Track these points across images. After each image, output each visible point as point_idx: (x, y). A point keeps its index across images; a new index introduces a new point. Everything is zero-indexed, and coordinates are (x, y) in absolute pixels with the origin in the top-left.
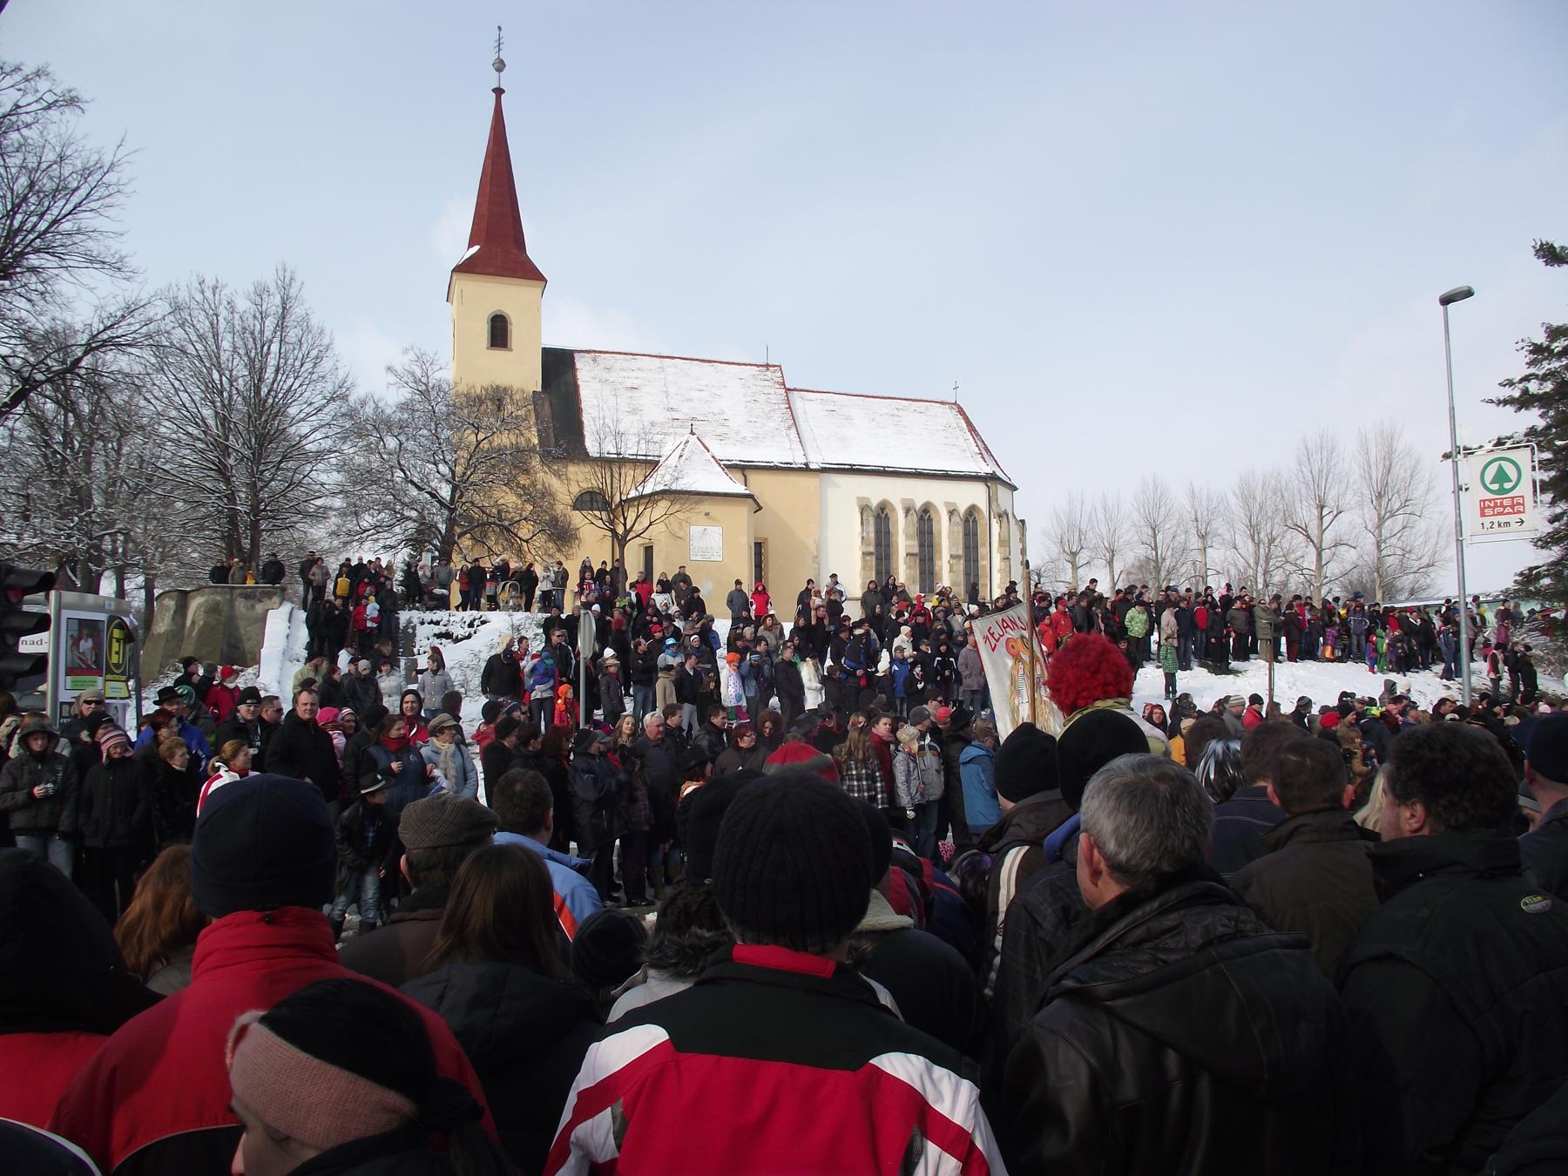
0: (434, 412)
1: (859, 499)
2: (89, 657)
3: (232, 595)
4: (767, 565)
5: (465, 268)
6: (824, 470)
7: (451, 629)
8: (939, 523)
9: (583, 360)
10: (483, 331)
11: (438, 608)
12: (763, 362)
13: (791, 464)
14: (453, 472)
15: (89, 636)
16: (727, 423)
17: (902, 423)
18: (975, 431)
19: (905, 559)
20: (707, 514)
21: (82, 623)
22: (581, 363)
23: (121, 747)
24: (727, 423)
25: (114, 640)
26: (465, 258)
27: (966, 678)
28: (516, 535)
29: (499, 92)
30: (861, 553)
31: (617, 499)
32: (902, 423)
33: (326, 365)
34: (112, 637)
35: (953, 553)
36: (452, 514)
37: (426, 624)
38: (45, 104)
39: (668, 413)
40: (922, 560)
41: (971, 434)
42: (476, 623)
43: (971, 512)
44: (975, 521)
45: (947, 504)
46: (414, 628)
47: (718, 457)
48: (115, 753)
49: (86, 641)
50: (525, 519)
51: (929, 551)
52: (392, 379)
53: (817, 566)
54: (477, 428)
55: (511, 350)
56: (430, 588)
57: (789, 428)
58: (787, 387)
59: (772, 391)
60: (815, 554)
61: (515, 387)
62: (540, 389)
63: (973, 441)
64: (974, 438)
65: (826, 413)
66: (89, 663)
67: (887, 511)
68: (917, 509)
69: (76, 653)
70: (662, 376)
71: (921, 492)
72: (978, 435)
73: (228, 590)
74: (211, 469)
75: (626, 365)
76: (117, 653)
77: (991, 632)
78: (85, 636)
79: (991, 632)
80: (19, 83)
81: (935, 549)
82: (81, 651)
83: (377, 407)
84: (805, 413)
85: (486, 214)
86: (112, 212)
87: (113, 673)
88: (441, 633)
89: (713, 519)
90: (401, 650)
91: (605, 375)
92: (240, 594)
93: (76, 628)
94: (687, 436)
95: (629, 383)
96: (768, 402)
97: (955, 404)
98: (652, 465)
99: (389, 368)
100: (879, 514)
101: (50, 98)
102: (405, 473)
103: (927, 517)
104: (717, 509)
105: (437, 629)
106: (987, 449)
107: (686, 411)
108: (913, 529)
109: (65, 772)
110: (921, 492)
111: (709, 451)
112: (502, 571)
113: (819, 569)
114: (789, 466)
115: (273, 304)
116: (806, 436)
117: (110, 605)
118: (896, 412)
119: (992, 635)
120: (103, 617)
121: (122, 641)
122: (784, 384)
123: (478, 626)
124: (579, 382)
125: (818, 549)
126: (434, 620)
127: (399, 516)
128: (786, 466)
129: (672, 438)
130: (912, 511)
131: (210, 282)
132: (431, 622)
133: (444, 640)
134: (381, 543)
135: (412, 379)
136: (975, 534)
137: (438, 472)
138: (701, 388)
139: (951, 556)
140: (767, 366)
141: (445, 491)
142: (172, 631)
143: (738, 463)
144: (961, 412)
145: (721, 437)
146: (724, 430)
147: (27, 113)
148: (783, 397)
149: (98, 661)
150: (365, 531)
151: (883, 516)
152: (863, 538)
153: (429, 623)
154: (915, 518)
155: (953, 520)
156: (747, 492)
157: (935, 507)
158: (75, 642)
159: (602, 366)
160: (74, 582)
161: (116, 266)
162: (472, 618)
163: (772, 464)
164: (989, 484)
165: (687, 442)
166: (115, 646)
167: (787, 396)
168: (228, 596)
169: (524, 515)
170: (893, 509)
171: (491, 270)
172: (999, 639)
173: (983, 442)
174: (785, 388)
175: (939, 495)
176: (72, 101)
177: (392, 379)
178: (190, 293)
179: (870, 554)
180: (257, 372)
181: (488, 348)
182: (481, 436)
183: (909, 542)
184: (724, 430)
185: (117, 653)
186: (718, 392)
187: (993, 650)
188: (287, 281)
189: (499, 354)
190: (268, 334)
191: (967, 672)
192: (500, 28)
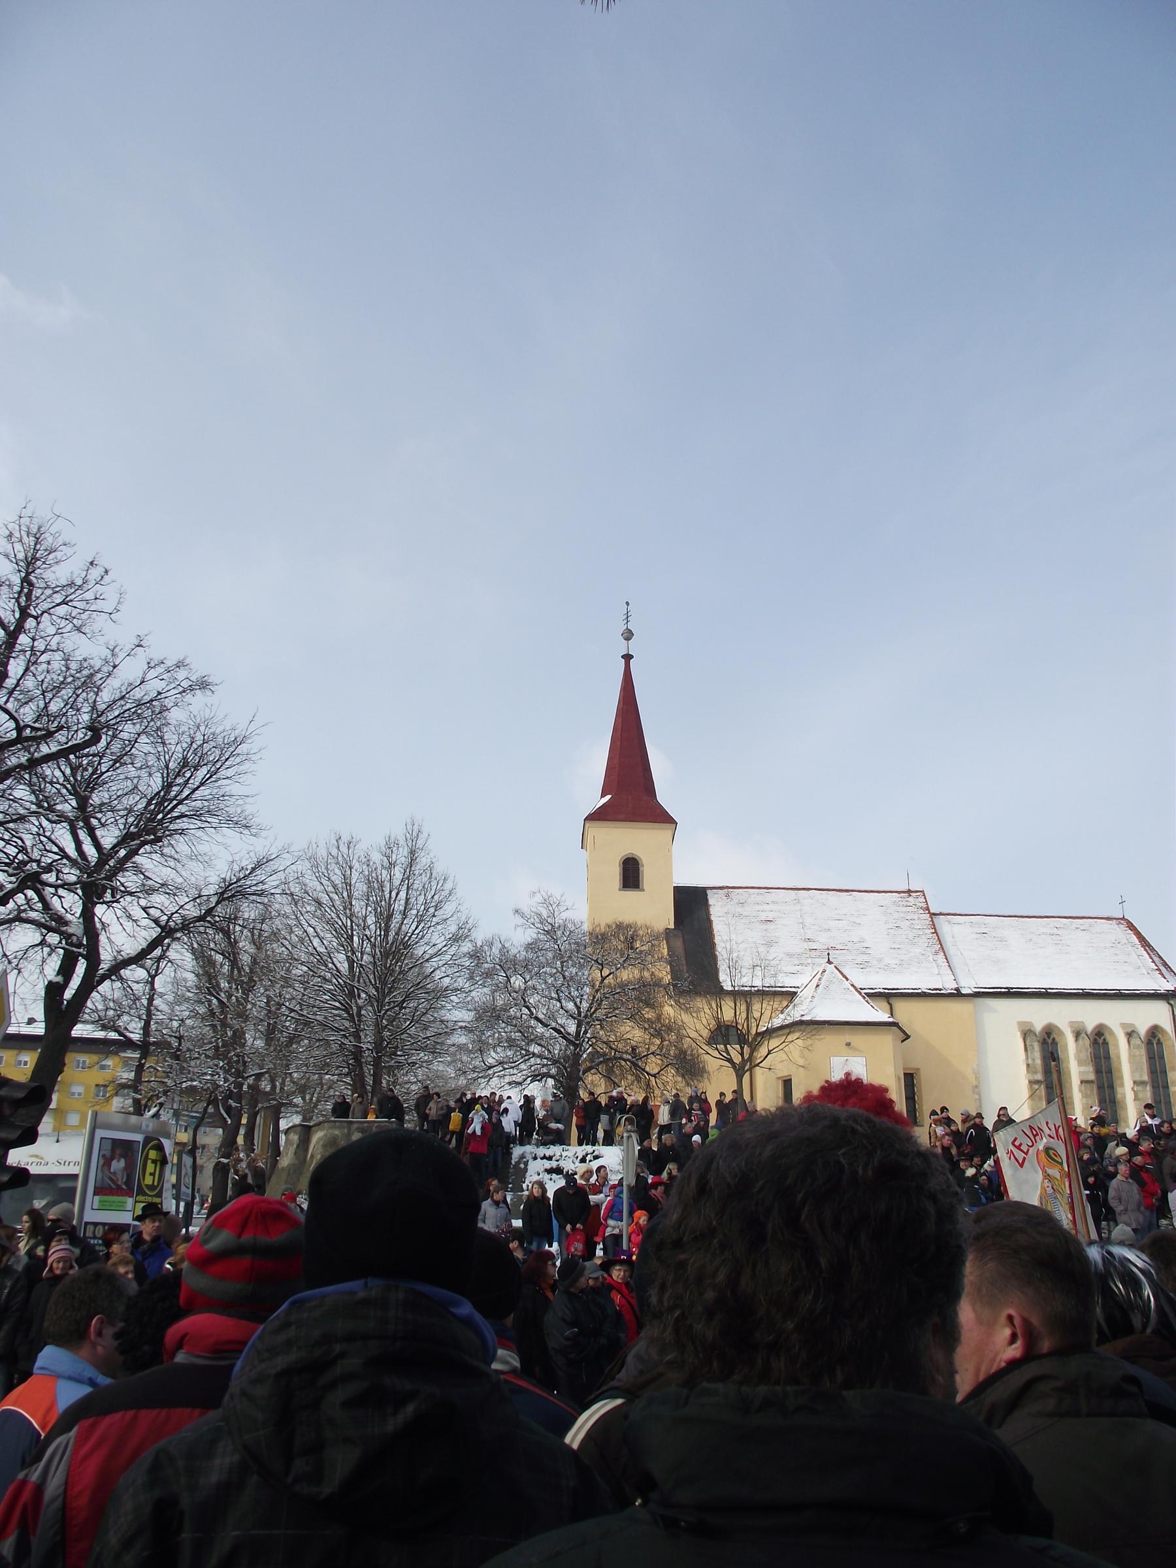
0: (560, 950)
1: (1020, 1024)
2: (120, 1178)
3: (349, 1129)
4: (920, 1097)
5: (597, 816)
6: (977, 995)
7: (562, 1164)
8: (1117, 1046)
9: (716, 896)
10: (615, 873)
11: (553, 1143)
12: (905, 888)
13: (940, 990)
14: (578, 1008)
15: (121, 1156)
16: (869, 951)
17: (1063, 942)
18: (1149, 946)
19: (1080, 1086)
20: (848, 1044)
21: (116, 1143)
22: (713, 899)
23: (65, 1262)
24: (869, 951)
25: (149, 1162)
26: (597, 807)
27: (1120, 1214)
28: (644, 1070)
29: (628, 658)
30: (1027, 1082)
31: (753, 1031)
32: (1063, 942)
33: (448, 909)
34: (147, 1158)
35: (1136, 1079)
36: (575, 1050)
37: (539, 1159)
38: (181, 689)
39: (806, 943)
40: (1100, 1088)
41: (1146, 950)
42: (588, 1158)
43: (1153, 1033)
44: (1159, 1043)
45: (1123, 1025)
46: (526, 1164)
47: (858, 986)
48: (57, 1268)
49: (118, 1161)
50: (653, 1053)
51: (1107, 1078)
52: (520, 921)
53: (977, 1097)
54: (602, 965)
55: (643, 890)
56: (546, 1123)
57: (936, 953)
58: (932, 912)
59: (916, 917)
60: (974, 1083)
61: (639, 924)
62: (672, 926)
63: (1147, 956)
64: (1149, 954)
65: (976, 936)
66: (119, 1183)
67: (1054, 1035)
68: (1089, 1033)
69: (106, 1172)
70: (798, 908)
71: (1092, 1014)
72: (1153, 950)
73: (346, 1125)
74: (338, 1008)
75: (760, 898)
76: (153, 1174)
77: (1017, 1143)
78: (117, 1157)
79: (1017, 1143)
80: (161, 674)
81: (1115, 1074)
82: (112, 1170)
83: (504, 946)
84: (953, 937)
85: (617, 766)
86: (243, 778)
87: (145, 1194)
88: (552, 1168)
89: (855, 1049)
90: (510, 1186)
91: (739, 909)
92: (358, 1128)
93: (109, 1147)
94: (824, 965)
95: (763, 916)
96: (912, 928)
97: (1123, 919)
98: (791, 995)
99: (517, 911)
100: (1044, 1039)
101: (185, 684)
102: (530, 1010)
103: (1101, 1041)
104: (859, 1039)
105: (548, 1164)
106: (1165, 964)
107: (823, 940)
108: (1087, 1054)
109: (12, 1288)
110: (1092, 1014)
111: (847, 979)
112: (618, 1105)
113: (980, 1099)
114: (938, 992)
115: (401, 855)
116: (955, 961)
117: (147, 1126)
118: (1055, 931)
119: (1019, 1148)
120: (139, 1137)
121: (158, 1163)
122: (928, 909)
123: (590, 1161)
124: (712, 918)
125: (977, 1078)
126: (547, 1155)
127: (523, 1052)
128: (912, 991)
129: (810, 968)
130: (1083, 1035)
131: (345, 838)
132: (544, 1157)
133: (554, 1176)
134: (507, 1079)
135: (537, 920)
136: (1162, 1057)
137: (562, 1008)
138: (838, 917)
139: (1135, 1082)
140: (909, 892)
141: (572, 1028)
142: (293, 1164)
143: (882, 991)
144: (1131, 926)
145: (863, 966)
146: (865, 958)
147: (166, 698)
148: (928, 922)
149: (129, 1182)
150: (490, 1068)
151: (1050, 1041)
152: (1028, 1065)
153: (542, 1159)
154: (1087, 1042)
155: (1132, 1042)
156: (891, 1020)
157: (1111, 1030)
158: (107, 1162)
159: (735, 901)
160: (225, 1119)
161: (242, 824)
162: (584, 1153)
163: (919, 991)
164: (1172, 1002)
165: (824, 971)
166: (150, 1167)
167: (932, 921)
168: (346, 1131)
169: (653, 1048)
170: (1061, 1033)
171: (622, 816)
172: (1028, 1150)
173: (1160, 957)
174: (929, 913)
175: (1112, 1015)
176: (203, 685)
177: (519, 920)
178: (328, 849)
179: (1038, 1082)
180: (386, 918)
181: (620, 890)
182: (606, 972)
183: (1083, 1069)
184: (865, 958)
185: (153, 1174)
186: (858, 921)
187: (1021, 1165)
188: (415, 834)
189: (631, 894)
190: (397, 882)
191: (1121, 1208)
192: (628, 604)
